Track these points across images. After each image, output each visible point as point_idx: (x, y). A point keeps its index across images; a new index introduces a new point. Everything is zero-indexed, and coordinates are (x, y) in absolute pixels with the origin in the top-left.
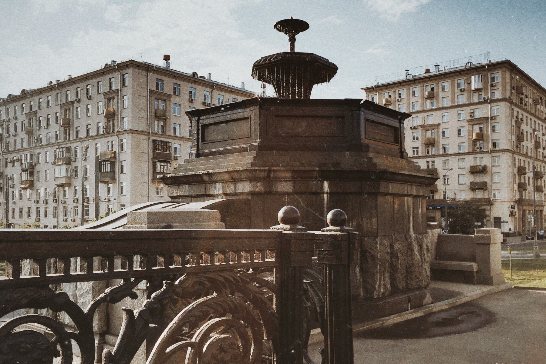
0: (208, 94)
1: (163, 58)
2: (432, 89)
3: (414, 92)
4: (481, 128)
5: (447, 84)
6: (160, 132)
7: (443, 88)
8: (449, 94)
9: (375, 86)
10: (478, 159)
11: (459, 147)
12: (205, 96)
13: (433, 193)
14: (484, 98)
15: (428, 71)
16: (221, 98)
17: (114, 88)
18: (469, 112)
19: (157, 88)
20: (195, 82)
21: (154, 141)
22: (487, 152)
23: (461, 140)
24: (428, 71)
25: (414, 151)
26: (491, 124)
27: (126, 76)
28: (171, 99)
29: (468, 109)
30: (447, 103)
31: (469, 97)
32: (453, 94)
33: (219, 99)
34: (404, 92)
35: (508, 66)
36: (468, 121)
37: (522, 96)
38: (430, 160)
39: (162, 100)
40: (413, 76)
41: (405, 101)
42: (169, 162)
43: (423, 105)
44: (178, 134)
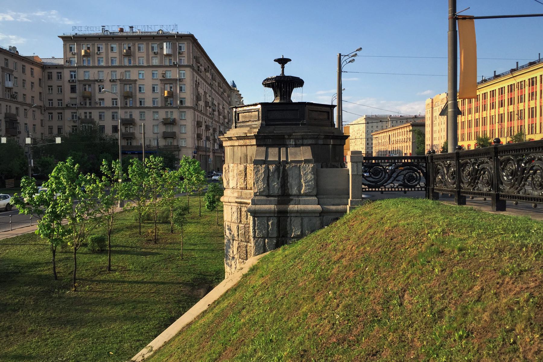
2: (129, 48)
3: (112, 48)
4: (171, 88)
5: (143, 46)
7: (139, 49)
8: (144, 55)
9: (74, 36)
10: (169, 113)
11: (154, 102)
14: (174, 63)
15: (122, 30)
18: (161, 72)
22: (176, 108)
24: (122, 30)
26: (179, 84)
29: (160, 71)
31: (161, 61)
32: (148, 55)
34: (103, 46)
35: (191, 38)
36: (161, 80)
37: (199, 65)
38: (128, 111)
40: (110, 33)
43: (120, 61)
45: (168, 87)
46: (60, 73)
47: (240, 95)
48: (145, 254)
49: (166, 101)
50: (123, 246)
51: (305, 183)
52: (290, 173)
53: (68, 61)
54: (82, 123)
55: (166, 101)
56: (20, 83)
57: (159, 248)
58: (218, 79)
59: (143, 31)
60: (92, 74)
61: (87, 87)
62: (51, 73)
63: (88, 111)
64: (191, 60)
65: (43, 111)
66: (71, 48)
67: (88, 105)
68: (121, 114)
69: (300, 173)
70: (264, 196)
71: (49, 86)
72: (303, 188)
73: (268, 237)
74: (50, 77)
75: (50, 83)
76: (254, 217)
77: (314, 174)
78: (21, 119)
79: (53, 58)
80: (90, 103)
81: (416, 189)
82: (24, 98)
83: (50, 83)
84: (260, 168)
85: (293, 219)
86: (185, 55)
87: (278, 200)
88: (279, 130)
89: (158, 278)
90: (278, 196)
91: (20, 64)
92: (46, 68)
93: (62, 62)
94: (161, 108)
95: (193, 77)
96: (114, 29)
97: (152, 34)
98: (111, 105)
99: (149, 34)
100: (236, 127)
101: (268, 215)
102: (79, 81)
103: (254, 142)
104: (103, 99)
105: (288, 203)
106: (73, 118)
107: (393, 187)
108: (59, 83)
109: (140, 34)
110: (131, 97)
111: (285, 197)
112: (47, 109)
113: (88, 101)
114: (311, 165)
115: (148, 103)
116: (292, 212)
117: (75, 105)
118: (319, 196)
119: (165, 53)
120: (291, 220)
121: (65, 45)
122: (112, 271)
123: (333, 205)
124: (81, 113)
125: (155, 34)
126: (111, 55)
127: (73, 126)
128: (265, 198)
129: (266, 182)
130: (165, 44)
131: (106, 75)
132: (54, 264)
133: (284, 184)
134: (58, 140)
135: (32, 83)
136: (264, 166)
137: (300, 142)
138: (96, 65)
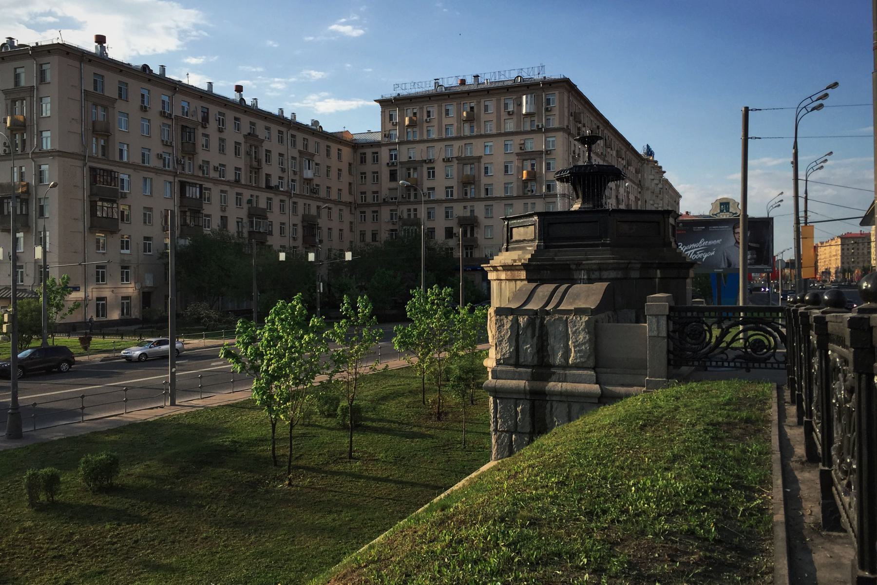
0: (166, 99)
1: (94, 39)
2: (472, 108)
3: (447, 111)
4: (533, 165)
5: (492, 104)
6: (100, 156)
7: (486, 108)
8: (493, 118)
9: (395, 98)
10: (529, 205)
11: (506, 189)
12: (163, 102)
13: (471, 249)
14: (538, 126)
15: (463, 82)
16: (186, 107)
17: (23, 83)
18: (519, 142)
19: (95, 88)
20: (149, 80)
21: (93, 170)
22: (540, 197)
23: (508, 179)
24: (463, 82)
25: (447, 192)
26: (546, 159)
27: (44, 67)
28: (116, 105)
29: (518, 140)
30: (492, 129)
31: (518, 125)
32: (499, 118)
33: (183, 108)
34: (434, 110)
35: (566, 85)
36: (518, 154)
37: (580, 125)
38: (468, 204)
39: (102, 106)
40: (446, 88)
41: (435, 123)
42: (114, 201)
43: (459, 129)
44: (125, 159)
45: (528, 164)
46: (377, 153)
47: (661, 167)
48: (413, 436)
49: (525, 187)
50: (389, 421)
51: (575, 347)
52: (551, 330)
53: (386, 135)
54: (404, 224)
55: (525, 187)
56: (323, 170)
57: (440, 428)
58: (616, 144)
59: (493, 80)
60: (417, 153)
61: (412, 170)
62: (365, 154)
63: (412, 207)
64: (566, 119)
65: (353, 209)
66: (391, 116)
67: (412, 199)
68: (459, 210)
69: (567, 330)
70: (511, 365)
71: (362, 173)
72: (572, 355)
73: (515, 432)
74: (363, 160)
75: (363, 168)
76: (495, 398)
77: (589, 333)
78: (323, 222)
79: (369, 132)
80: (416, 195)
81: (769, 366)
82: (329, 193)
83: (363, 168)
84: (505, 321)
85: (555, 405)
86: (556, 112)
87: (532, 373)
88: (566, 256)
89: (410, 477)
90: (533, 367)
91: (323, 144)
92: (359, 148)
93: (379, 138)
94: (518, 197)
95: (569, 146)
96: (451, 82)
97: (506, 84)
98: (444, 197)
99: (501, 84)
100: (507, 250)
101: (515, 396)
102: (401, 163)
103: (523, 274)
104: (433, 189)
105: (547, 378)
106: (392, 218)
107: (726, 360)
108: (375, 168)
109: (489, 86)
110: (474, 184)
111: (543, 368)
112: (358, 207)
113: (412, 193)
114: (585, 318)
115: (498, 191)
116: (553, 393)
117: (396, 198)
118: (598, 370)
119: (524, 112)
120: (552, 407)
121: (383, 112)
122: (355, 459)
123: (623, 385)
124: (403, 210)
125: (510, 83)
126: (446, 121)
127: (392, 230)
128: (512, 368)
129: (514, 343)
130: (524, 97)
131: (437, 152)
132: (274, 443)
133: (542, 349)
134: (348, 256)
135: (340, 170)
136: (510, 318)
137: (596, 275)
138: (425, 137)
